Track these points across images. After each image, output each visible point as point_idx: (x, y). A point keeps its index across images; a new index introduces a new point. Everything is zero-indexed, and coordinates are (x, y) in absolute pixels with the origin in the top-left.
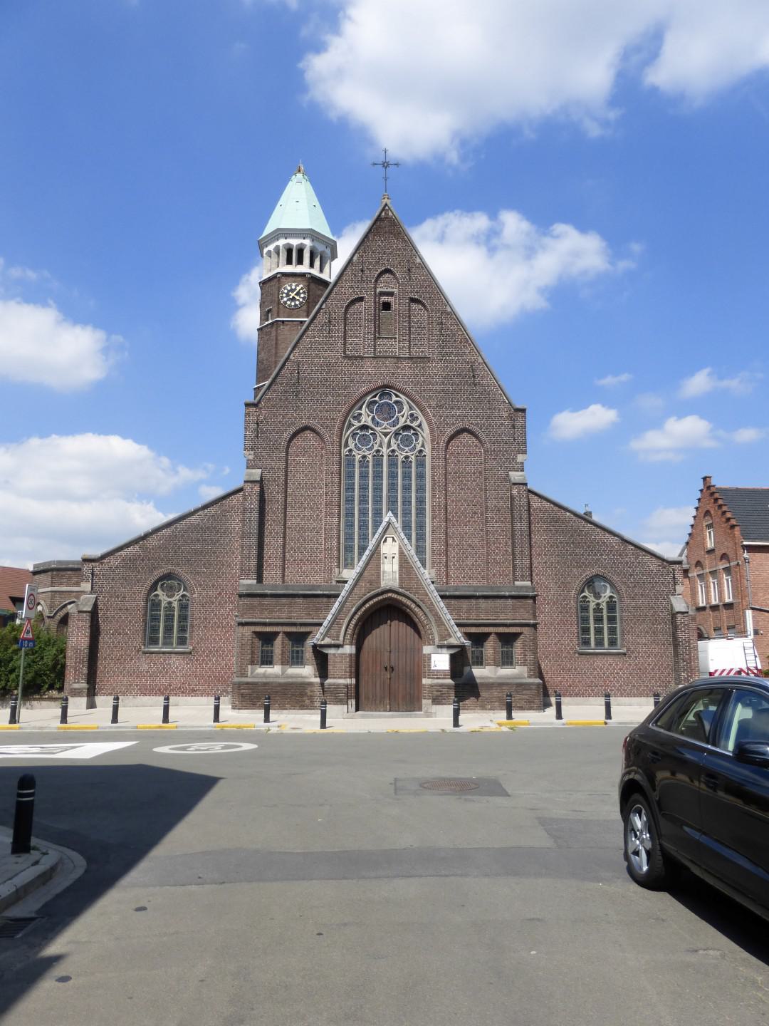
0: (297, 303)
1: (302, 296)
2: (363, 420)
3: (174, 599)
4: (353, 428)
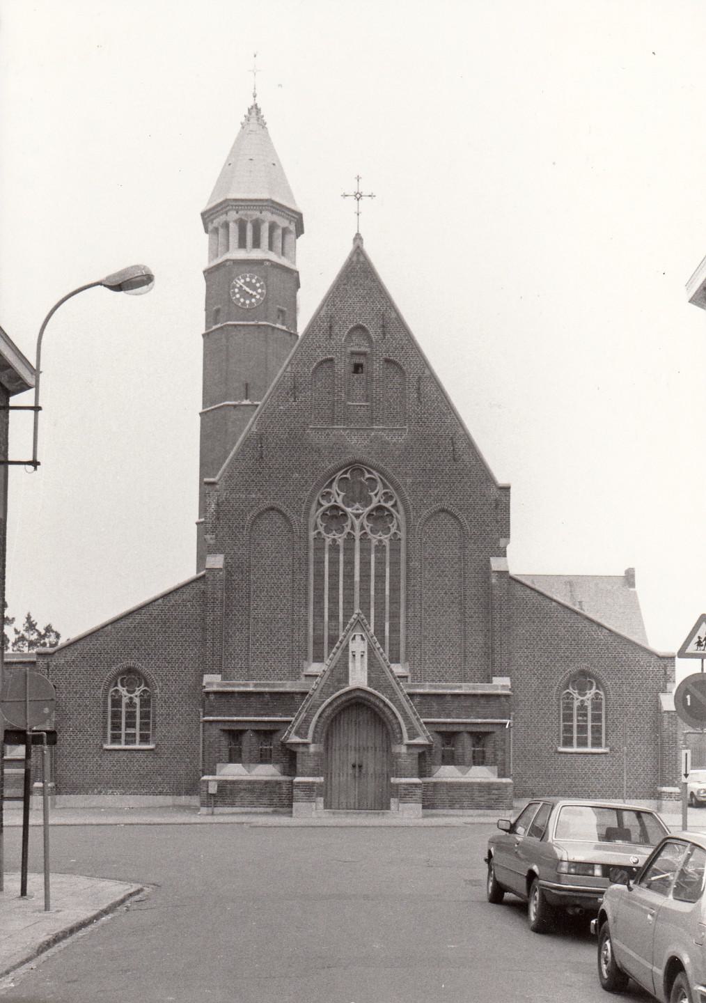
0: (253, 300)
1: (259, 291)
2: (333, 500)
4: (322, 509)
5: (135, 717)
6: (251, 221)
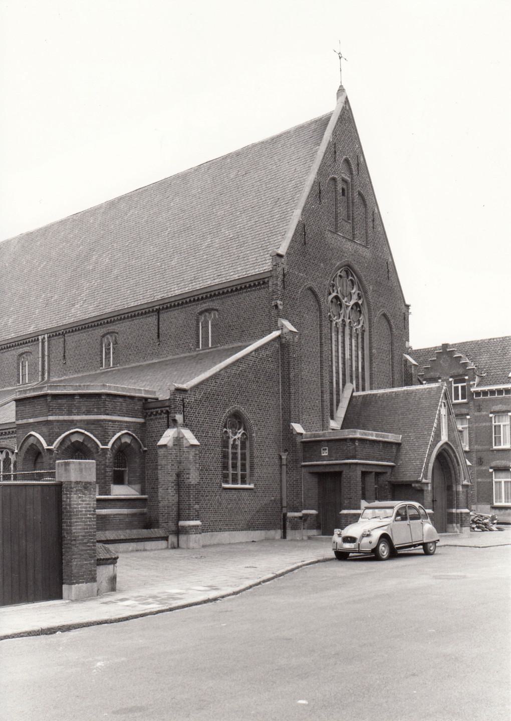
3: (233, 439)
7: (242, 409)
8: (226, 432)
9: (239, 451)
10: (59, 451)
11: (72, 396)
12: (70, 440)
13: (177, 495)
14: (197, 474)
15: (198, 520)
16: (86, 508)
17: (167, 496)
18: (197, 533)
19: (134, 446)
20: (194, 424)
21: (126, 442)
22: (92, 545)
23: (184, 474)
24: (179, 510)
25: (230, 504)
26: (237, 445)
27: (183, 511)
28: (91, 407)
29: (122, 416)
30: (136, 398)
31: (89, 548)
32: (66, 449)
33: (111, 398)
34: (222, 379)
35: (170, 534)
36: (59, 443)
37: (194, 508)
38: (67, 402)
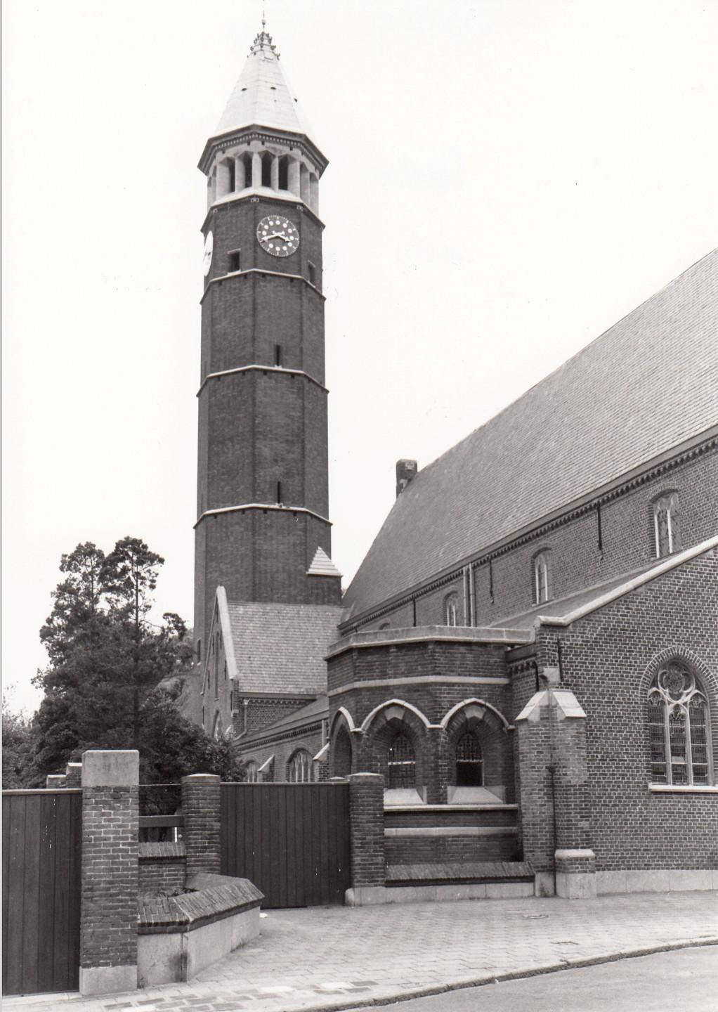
0: (285, 248)
1: (292, 238)
3: (672, 706)
5: (684, 739)
6: (279, 157)
7: (689, 653)
8: (656, 693)
9: (688, 726)
10: (370, 735)
11: (385, 649)
12: (385, 718)
13: (551, 803)
14: (583, 767)
15: (589, 848)
16: (117, 832)
17: (534, 804)
18: (586, 872)
19: (490, 724)
20: (583, 682)
21: (474, 718)
22: (127, 898)
23: (560, 767)
24: (555, 830)
25: (667, 820)
26: (683, 716)
27: (561, 832)
28: (412, 664)
29: (465, 675)
30: (492, 646)
31: (121, 904)
32: (379, 732)
33: (444, 647)
34: (640, 603)
35: (538, 871)
36: (369, 723)
37: (580, 826)
38: (379, 657)
